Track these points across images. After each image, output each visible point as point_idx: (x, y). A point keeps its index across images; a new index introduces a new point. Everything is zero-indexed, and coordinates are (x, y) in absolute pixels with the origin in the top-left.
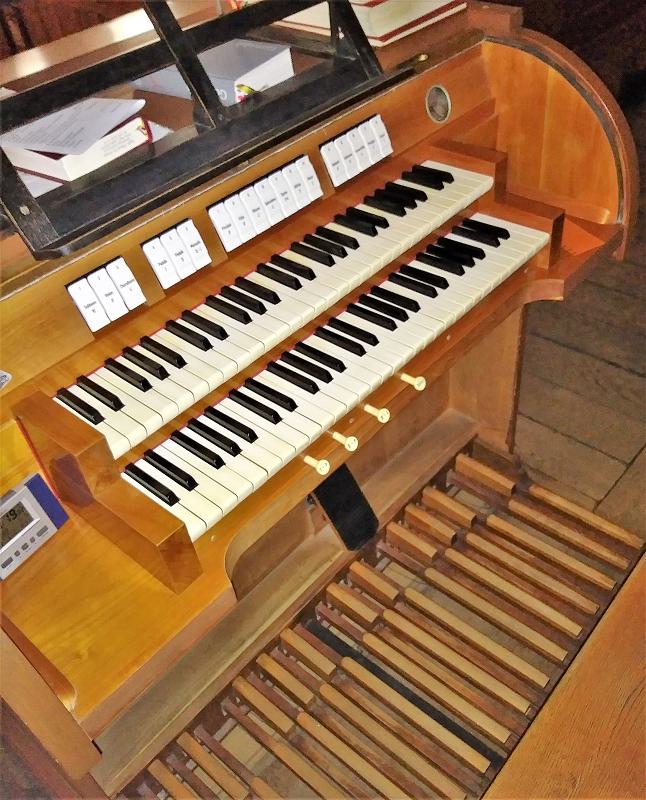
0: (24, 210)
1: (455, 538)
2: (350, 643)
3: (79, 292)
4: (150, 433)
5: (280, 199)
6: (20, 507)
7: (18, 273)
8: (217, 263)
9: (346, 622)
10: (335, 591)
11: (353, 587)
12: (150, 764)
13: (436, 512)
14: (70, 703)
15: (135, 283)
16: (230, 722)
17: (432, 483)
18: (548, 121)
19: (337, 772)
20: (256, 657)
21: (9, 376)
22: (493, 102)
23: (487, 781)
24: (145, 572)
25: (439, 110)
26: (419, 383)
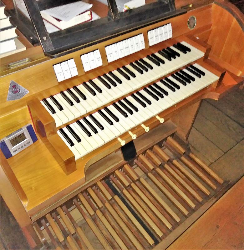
0: (45, 38)
1: (160, 165)
2: (118, 190)
3: (57, 68)
4: (70, 121)
5: (130, 47)
6: (23, 134)
7: (39, 59)
8: (104, 65)
9: (118, 183)
10: (117, 172)
11: (123, 172)
12: (46, 214)
13: (157, 154)
14: (25, 204)
15: (76, 68)
16: (74, 206)
17: (157, 144)
18: (229, 35)
19: (105, 232)
20: (88, 188)
21: (28, 92)
22: (211, 25)
23: (151, 247)
24: (58, 165)
25: (192, 24)
26: (162, 120)
